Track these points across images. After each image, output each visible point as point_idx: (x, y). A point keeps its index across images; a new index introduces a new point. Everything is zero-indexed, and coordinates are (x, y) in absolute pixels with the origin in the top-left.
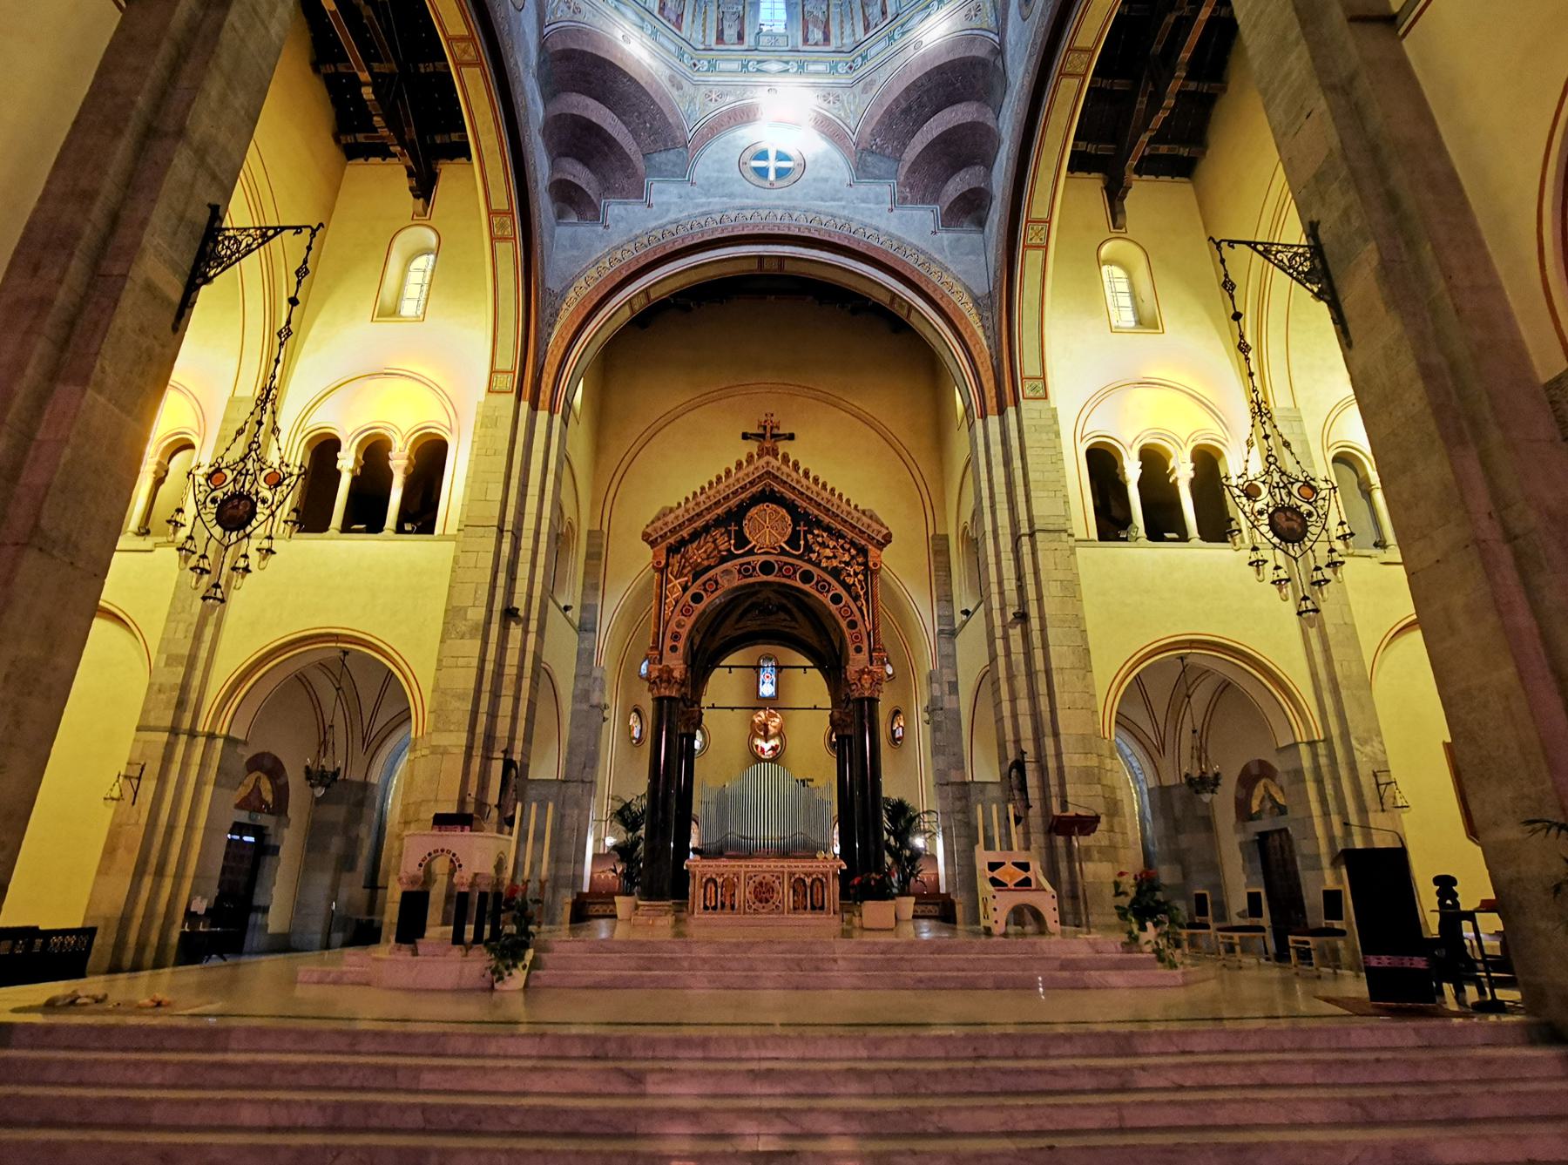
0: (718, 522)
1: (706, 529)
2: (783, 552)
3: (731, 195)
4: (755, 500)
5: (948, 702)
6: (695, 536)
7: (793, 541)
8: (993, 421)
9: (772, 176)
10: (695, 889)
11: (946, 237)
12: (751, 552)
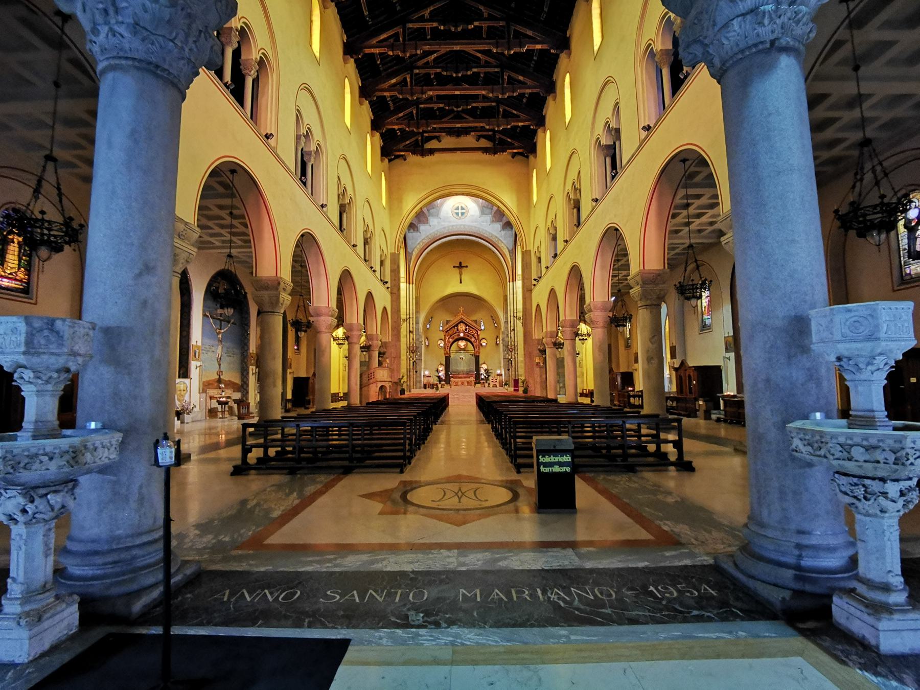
3: (450, 222)
4: (460, 323)
8: (511, 283)
10: (453, 384)
11: (503, 233)
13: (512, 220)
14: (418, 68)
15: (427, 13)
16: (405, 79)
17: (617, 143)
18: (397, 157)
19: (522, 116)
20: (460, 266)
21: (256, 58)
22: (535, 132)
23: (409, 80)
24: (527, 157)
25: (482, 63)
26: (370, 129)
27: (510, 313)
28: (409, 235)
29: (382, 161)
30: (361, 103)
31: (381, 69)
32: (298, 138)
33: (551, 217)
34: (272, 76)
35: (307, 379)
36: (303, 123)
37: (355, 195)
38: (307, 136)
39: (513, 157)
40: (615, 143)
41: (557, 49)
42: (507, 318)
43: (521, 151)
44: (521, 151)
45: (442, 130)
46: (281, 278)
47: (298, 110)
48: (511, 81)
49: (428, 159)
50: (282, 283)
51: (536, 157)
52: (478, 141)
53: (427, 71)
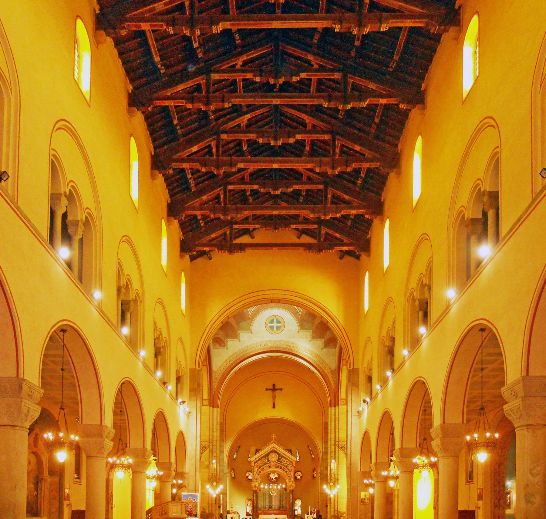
0: (264, 457)
1: (262, 458)
2: (276, 463)
5: (325, 472)
6: (259, 460)
7: (278, 460)
9: (275, 321)
11: (325, 350)
12: (270, 463)
13: (337, 332)
14: (224, 132)
15: (239, 62)
16: (209, 146)
17: (491, 214)
18: (202, 254)
19: (356, 201)
20: (274, 389)
21: (65, 192)
22: (370, 223)
23: (222, 196)
24: (358, 257)
25: (309, 127)
26: (166, 214)
27: (331, 443)
28: (214, 352)
29: (181, 256)
30: (153, 177)
31: (179, 132)
32: (119, 290)
33: (388, 324)
34: (95, 232)
35: (84, 512)
36: (81, 205)
37: (169, 336)
38: (127, 286)
39: (341, 258)
40: (485, 214)
41: (409, 103)
42: (326, 448)
43: (351, 248)
44: (351, 248)
45: (256, 218)
46: (24, 380)
47: (119, 263)
48: (346, 152)
49: (238, 256)
50: (25, 387)
51: (369, 256)
52: (299, 238)
53: (243, 187)
